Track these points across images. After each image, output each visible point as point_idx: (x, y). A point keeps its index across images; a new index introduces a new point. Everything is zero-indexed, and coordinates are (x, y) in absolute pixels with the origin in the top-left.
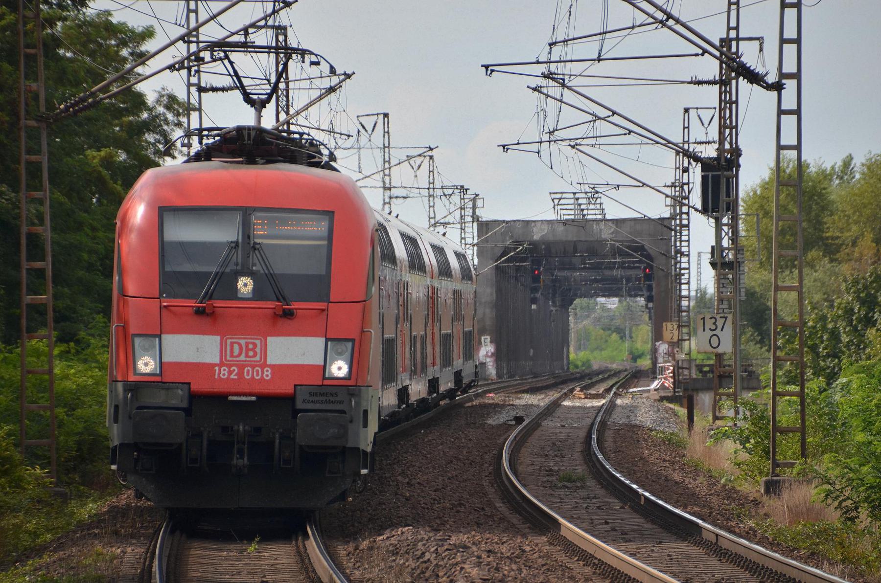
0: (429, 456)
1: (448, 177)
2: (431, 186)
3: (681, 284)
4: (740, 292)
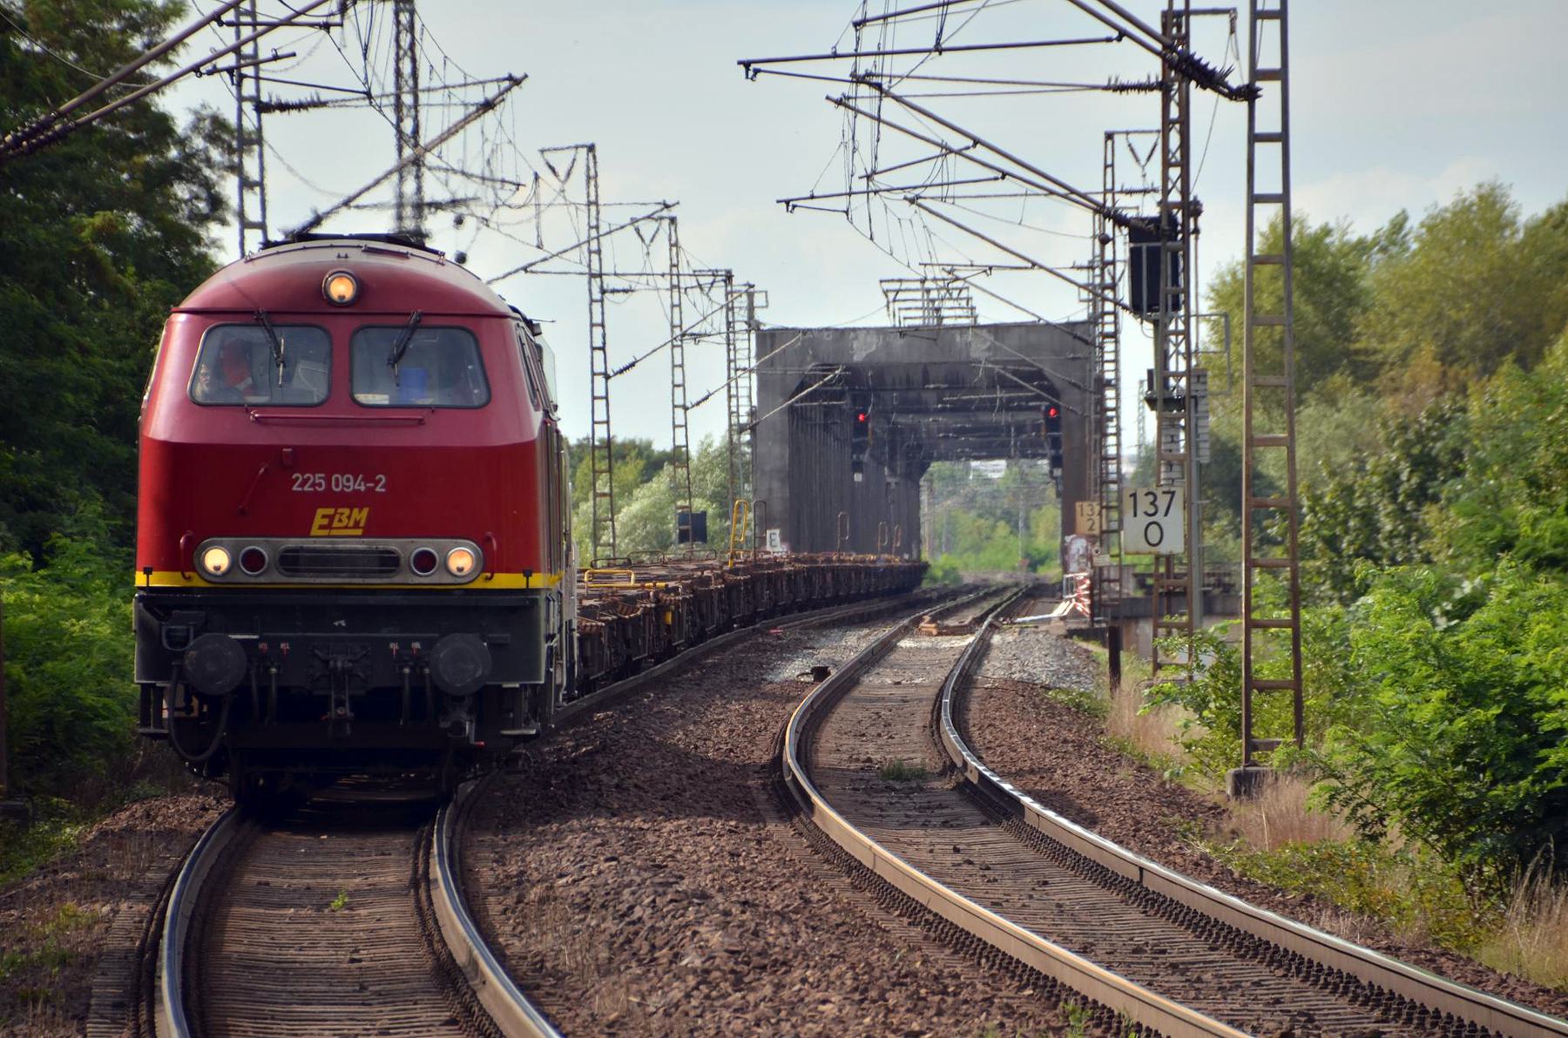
1: (701, 251)
3: (1105, 435)
4: (1198, 449)
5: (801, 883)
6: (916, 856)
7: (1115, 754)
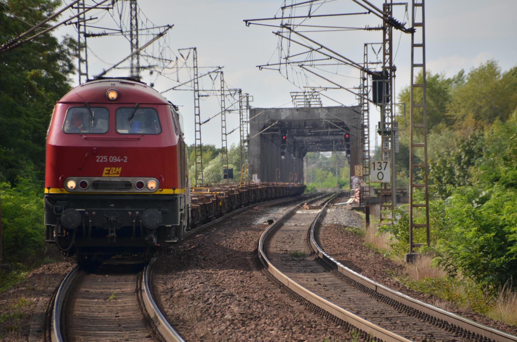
1: (231, 83)
4: (395, 148)
5: (264, 291)
6: (302, 282)
7: (368, 248)
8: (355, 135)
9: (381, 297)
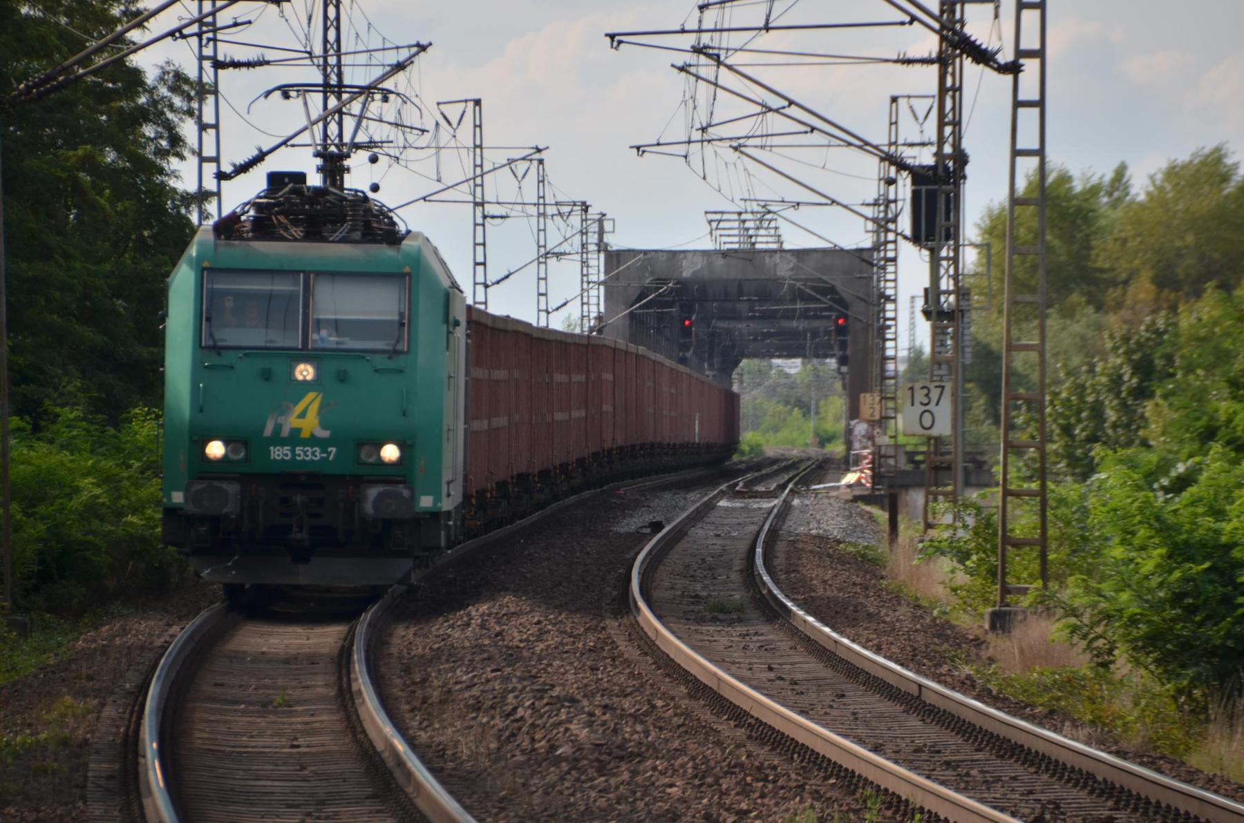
0: (528, 576)
1: (564, 187)
2: (541, 201)
3: (885, 340)
4: (963, 352)
6: (740, 673)
8: (861, 317)
9: (932, 711)
